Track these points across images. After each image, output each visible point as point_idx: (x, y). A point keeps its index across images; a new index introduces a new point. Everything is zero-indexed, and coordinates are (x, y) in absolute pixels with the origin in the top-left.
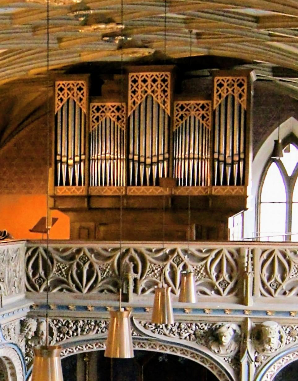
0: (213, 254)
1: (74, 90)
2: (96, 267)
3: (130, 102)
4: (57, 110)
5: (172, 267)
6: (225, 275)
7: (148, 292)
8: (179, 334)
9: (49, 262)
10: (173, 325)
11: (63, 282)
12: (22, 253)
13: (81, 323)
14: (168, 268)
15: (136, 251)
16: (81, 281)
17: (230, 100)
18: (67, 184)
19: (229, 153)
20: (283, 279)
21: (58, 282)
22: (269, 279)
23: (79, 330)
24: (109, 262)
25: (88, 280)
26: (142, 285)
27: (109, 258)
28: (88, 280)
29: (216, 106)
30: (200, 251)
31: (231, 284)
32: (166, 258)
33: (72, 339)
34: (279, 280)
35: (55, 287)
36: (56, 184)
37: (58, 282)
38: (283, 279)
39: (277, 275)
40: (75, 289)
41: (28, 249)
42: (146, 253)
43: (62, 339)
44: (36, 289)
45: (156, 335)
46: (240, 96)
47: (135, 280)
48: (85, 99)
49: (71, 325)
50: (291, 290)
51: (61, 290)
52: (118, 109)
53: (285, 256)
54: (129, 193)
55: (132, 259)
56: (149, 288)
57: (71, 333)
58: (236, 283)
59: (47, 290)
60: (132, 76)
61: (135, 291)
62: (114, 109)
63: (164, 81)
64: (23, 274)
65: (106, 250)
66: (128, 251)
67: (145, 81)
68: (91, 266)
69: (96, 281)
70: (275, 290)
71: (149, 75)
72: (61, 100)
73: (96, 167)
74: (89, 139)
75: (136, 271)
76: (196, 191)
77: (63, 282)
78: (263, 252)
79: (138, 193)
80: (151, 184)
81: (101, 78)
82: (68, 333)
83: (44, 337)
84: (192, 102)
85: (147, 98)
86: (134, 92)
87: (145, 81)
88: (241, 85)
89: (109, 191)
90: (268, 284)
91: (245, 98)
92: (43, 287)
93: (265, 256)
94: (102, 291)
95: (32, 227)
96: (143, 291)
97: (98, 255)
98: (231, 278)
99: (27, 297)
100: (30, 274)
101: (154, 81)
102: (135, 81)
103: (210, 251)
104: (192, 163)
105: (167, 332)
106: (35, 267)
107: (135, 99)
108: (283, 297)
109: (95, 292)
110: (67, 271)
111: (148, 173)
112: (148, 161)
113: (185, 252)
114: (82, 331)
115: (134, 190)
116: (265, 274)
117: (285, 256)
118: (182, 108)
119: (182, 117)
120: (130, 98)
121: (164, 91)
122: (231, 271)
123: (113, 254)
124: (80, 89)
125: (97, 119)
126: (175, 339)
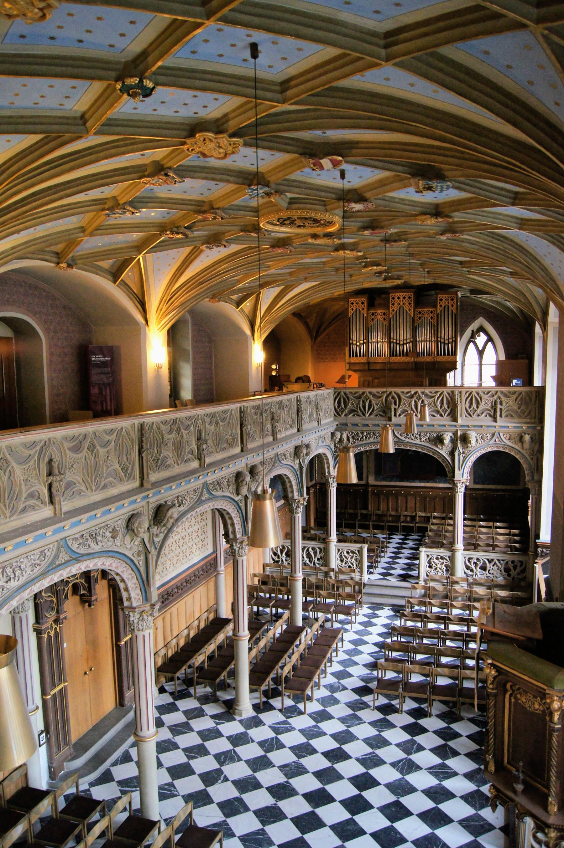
0: (438, 394)
1: (358, 305)
2: (373, 402)
3: (391, 310)
4: (350, 314)
5: (415, 402)
6: (445, 406)
11: (355, 411)
14: (413, 402)
16: (365, 410)
17: (446, 308)
18: (356, 356)
19: (446, 337)
20: (478, 407)
22: (470, 407)
25: (369, 410)
26: (399, 412)
30: (431, 392)
32: (412, 397)
33: (360, 443)
35: (350, 414)
36: (350, 356)
38: (478, 407)
39: (474, 405)
45: (407, 440)
46: (452, 306)
47: (395, 409)
48: (365, 309)
50: (482, 414)
51: (354, 415)
52: (384, 314)
53: (478, 394)
54: (391, 361)
55: (393, 398)
58: (451, 410)
60: (391, 295)
61: (395, 415)
63: (410, 298)
65: (378, 392)
67: (399, 298)
68: (370, 402)
71: (401, 295)
73: (372, 347)
74: (368, 331)
75: (395, 404)
76: (428, 359)
77: (355, 411)
80: (403, 355)
81: (375, 297)
86: (393, 304)
87: (399, 298)
88: (452, 300)
89: (380, 360)
91: (455, 307)
94: (376, 416)
95: (337, 380)
96: (400, 415)
97: (374, 396)
98: (448, 407)
99: (335, 419)
101: (404, 298)
102: (393, 298)
103: (436, 392)
104: (426, 344)
106: (339, 403)
107: (394, 308)
109: (372, 416)
111: (402, 349)
112: (402, 343)
113: (423, 393)
115: (394, 359)
117: (478, 394)
118: (420, 313)
119: (420, 318)
121: (410, 304)
122: (448, 403)
124: (363, 303)
125: (373, 320)
126: (418, 442)
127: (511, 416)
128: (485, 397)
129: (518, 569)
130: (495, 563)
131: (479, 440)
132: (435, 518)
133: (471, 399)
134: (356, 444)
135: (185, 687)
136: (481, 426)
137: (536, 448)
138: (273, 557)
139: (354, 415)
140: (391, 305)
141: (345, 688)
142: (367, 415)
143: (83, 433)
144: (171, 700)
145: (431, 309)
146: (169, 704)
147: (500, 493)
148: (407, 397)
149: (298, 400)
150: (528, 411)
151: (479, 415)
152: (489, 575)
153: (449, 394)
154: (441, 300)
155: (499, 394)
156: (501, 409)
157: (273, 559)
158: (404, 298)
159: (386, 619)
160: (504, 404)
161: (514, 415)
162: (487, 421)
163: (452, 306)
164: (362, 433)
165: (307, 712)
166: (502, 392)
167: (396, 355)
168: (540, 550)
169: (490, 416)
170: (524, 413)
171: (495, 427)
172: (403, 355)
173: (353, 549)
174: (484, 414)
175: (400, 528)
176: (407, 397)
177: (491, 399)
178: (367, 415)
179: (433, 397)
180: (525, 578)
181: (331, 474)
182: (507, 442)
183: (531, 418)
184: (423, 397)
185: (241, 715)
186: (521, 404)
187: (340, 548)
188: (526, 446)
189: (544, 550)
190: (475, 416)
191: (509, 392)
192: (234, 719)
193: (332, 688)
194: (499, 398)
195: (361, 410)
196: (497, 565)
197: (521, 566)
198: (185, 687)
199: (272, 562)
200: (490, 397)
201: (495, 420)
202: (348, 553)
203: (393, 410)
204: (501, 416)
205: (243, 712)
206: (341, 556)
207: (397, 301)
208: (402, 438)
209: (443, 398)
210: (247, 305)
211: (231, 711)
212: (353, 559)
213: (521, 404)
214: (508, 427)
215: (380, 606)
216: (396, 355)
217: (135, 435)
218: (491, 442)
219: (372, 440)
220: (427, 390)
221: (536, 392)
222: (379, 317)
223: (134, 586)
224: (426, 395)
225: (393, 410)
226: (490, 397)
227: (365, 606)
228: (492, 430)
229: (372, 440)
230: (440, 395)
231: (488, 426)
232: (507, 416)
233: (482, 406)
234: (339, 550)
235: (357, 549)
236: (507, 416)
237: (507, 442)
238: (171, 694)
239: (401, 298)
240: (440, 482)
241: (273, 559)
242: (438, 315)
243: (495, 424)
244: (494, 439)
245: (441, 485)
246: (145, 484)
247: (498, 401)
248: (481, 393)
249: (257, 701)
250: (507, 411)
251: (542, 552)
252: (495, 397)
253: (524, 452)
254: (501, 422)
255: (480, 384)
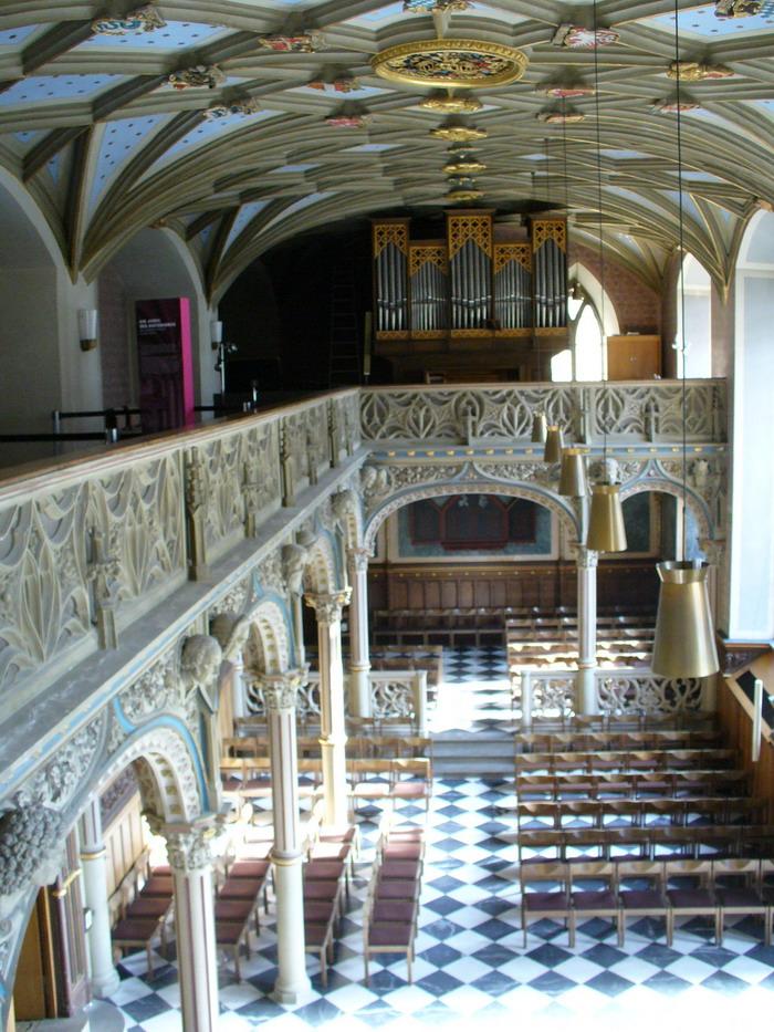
0: (550, 394)
2: (528, 409)
3: (451, 246)
5: (509, 409)
6: (562, 415)
7: (486, 435)
8: (520, 475)
9: (384, 408)
10: (106, 484)
11: (399, 429)
12: (357, 399)
13: (420, 470)
14: (411, 414)
15: (473, 394)
16: (419, 428)
18: (547, 325)
20: (617, 417)
21: (393, 430)
22: (604, 417)
23: (418, 476)
24: (446, 406)
25: (519, 424)
26: (480, 428)
27: (446, 402)
28: (426, 425)
29: (535, 250)
30: (536, 392)
31: (568, 424)
32: (503, 401)
33: (412, 486)
34: (564, 419)
35: (391, 433)
37: (393, 430)
38: (617, 417)
39: (612, 413)
40: (411, 435)
41: (362, 396)
42: (483, 396)
43: (400, 486)
44: (371, 437)
45: (497, 478)
46: (559, 240)
47: (473, 423)
48: (489, 244)
49: (410, 472)
50: (625, 427)
51: (397, 437)
52: (439, 252)
53: (618, 394)
55: (469, 403)
56: (487, 430)
57: (409, 480)
58: (573, 423)
59: (383, 436)
61: (474, 434)
62: (434, 253)
64: (358, 422)
65: (441, 394)
66: (464, 395)
68: (522, 408)
69: (433, 427)
70: (611, 428)
71: (470, 219)
72: (381, 244)
75: (474, 414)
77: (399, 429)
78: (598, 391)
79: (464, 336)
82: (406, 480)
83: (383, 486)
84: (512, 246)
85: (468, 241)
86: (455, 236)
88: (559, 229)
90: (603, 422)
91: (563, 242)
92: (380, 433)
93: (599, 394)
94: (439, 436)
96: (482, 433)
97: (434, 400)
98: (567, 417)
99: (362, 445)
100: (600, 418)
101: (475, 225)
102: (455, 225)
103: (546, 392)
105: (507, 473)
106: (370, 414)
107: (454, 244)
108: (617, 435)
109: (432, 437)
110: (404, 417)
111: (472, 315)
113: (522, 393)
114: (422, 477)
116: (601, 413)
117: (618, 394)
119: (502, 261)
120: (450, 241)
121: (485, 235)
122: (567, 411)
123: (542, 396)
124: (400, 233)
126: (515, 480)
127: (674, 430)
128: (628, 398)
129: (688, 692)
130: (650, 685)
131: (622, 473)
132: (510, 616)
133: (606, 405)
134: (403, 489)
135: (165, 962)
136: (626, 450)
137: (717, 482)
138: (251, 704)
139: (397, 437)
140: (450, 237)
141: (460, 929)
142: (422, 436)
143: (83, 483)
144: (146, 990)
145: (523, 245)
146: (145, 999)
147: (638, 566)
148: (399, 403)
149: (331, 408)
150: (701, 420)
151: (619, 431)
152: (640, 706)
153: (567, 395)
154: (381, 233)
155: (652, 393)
156: (657, 420)
157: (251, 711)
158: (475, 225)
159: (479, 799)
160: (661, 409)
161: (678, 428)
162: (632, 439)
163: (559, 240)
164: (414, 469)
165: (415, 979)
166: (657, 390)
167: (463, 327)
168: (729, 656)
169: (640, 431)
170: (694, 425)
171: (649, 449)
172: (475, 327)
173: (400, 681)
174: (628, 429)
175: (426, 639)
176: (399, 403)
177: (640, 401)
178: (422, 436)
179: (446, 402)
180: (698, 707)
181: (359, 545)
182: (668, 475)
183: (705, 433)
184: (523, 399)
185: (293, 1001)
186: (690, 409)
187: (375, 681)
188: (701, 480)
189: (737, 656)
190: (613, 433)
191: (669, 389)
192: (282, 1011)
193: (439, 932)
194: (654, 399)
195: (411, 428)
196: (653, 689)
197: (692, 686)
198: (165, 962)
199: (249, 714)
200: (637, 398)
201: (649, 439)
202: (391, 688)
203: (470, 425)
204: (657, 431)
205: (298, 996)
206: (377, 694)
207: (462, 231)
208: (488, 475)
209: (557, 402)
210: (205, 235)
211: (271, 996)
212: (402, 699)
213: (690, 409)
214: (671, 449)
215: (459, 779)
216: (463, 327)
217: (175, 479)
218: (642, 477)
219: (432, 480)
220: (434, 389)
221: (715, 389)
222: (513, 256)
223: (181, 764)
224: (529, 398)
225: (470, 425)
226: (637, 398)
227: (435, 780)
228: (644, 456)
229: (432, 480)
230: (554, 395)
231: (637, 450)
232: (667, 431)
233: (625, 414)
234: (374, 685)
235: (409, 680)
236: (667, 431)
237: (668, 475)
238: (143, 978)
239: (470, 226)
240: (515, 553)
241: (251, 711)
242: (534, 256)
243: (649, 445)
244: (646, 472)
245: (518, 558)
246: (199, 572)
247: (652, 405)
248: (622, 392)
249: (318, 970)
250: (666, 422)
251: (734, 659)
252: (646, 398)
253: (696, 491)
254: (657, 442)
255: (574, 377)
